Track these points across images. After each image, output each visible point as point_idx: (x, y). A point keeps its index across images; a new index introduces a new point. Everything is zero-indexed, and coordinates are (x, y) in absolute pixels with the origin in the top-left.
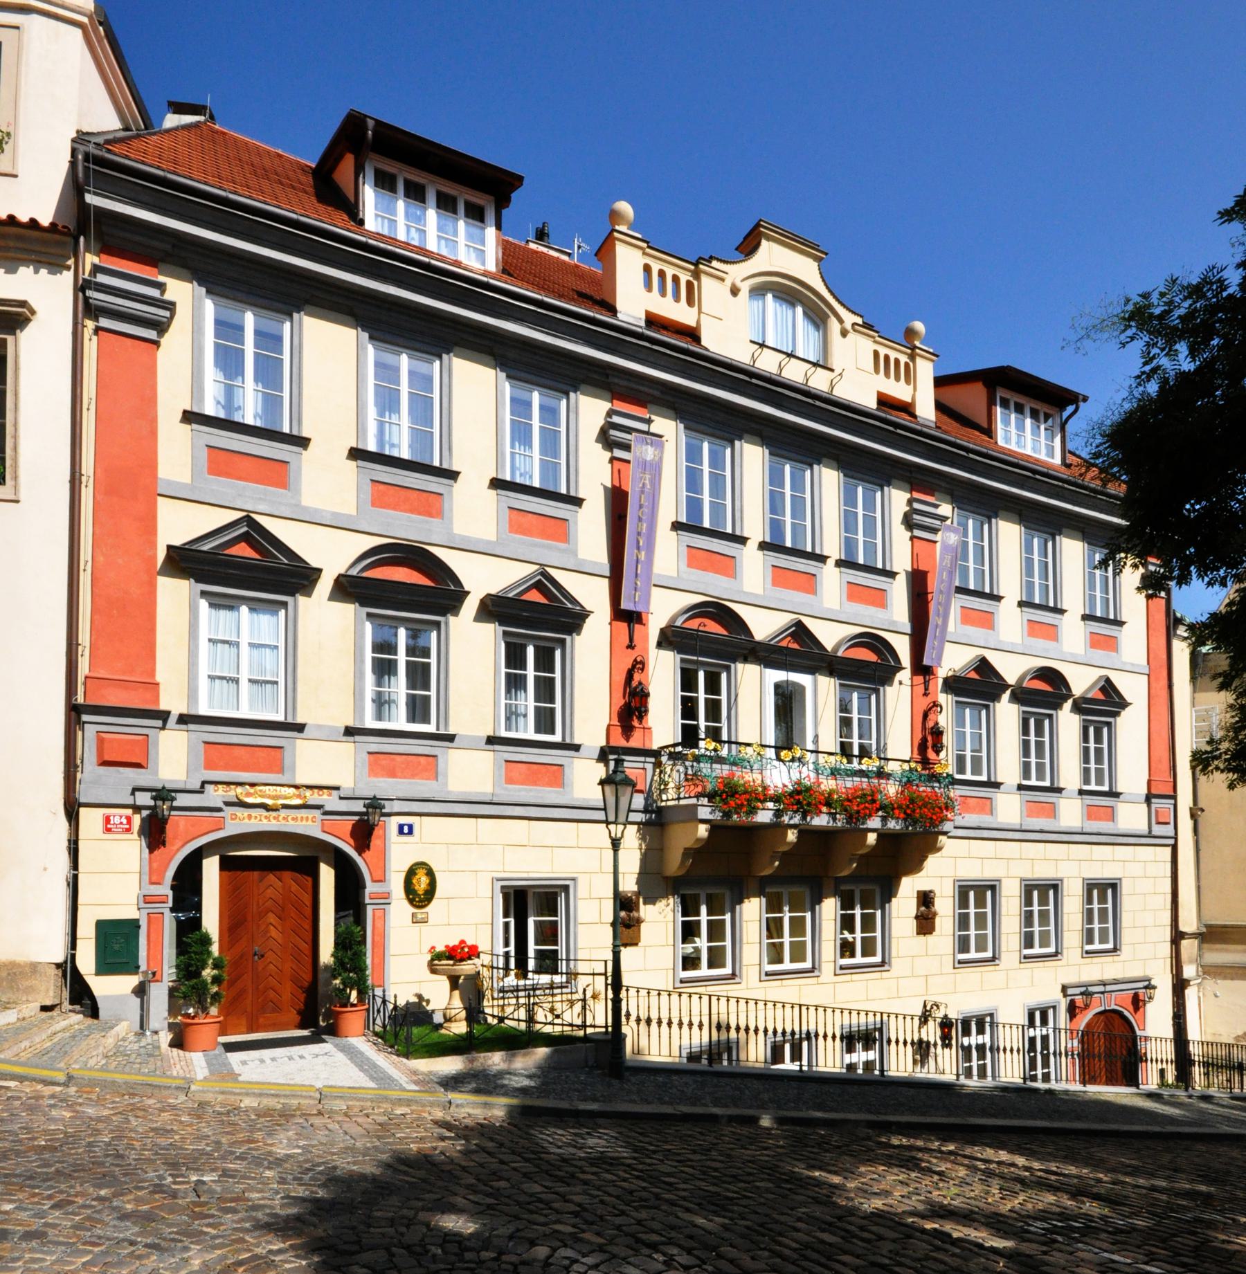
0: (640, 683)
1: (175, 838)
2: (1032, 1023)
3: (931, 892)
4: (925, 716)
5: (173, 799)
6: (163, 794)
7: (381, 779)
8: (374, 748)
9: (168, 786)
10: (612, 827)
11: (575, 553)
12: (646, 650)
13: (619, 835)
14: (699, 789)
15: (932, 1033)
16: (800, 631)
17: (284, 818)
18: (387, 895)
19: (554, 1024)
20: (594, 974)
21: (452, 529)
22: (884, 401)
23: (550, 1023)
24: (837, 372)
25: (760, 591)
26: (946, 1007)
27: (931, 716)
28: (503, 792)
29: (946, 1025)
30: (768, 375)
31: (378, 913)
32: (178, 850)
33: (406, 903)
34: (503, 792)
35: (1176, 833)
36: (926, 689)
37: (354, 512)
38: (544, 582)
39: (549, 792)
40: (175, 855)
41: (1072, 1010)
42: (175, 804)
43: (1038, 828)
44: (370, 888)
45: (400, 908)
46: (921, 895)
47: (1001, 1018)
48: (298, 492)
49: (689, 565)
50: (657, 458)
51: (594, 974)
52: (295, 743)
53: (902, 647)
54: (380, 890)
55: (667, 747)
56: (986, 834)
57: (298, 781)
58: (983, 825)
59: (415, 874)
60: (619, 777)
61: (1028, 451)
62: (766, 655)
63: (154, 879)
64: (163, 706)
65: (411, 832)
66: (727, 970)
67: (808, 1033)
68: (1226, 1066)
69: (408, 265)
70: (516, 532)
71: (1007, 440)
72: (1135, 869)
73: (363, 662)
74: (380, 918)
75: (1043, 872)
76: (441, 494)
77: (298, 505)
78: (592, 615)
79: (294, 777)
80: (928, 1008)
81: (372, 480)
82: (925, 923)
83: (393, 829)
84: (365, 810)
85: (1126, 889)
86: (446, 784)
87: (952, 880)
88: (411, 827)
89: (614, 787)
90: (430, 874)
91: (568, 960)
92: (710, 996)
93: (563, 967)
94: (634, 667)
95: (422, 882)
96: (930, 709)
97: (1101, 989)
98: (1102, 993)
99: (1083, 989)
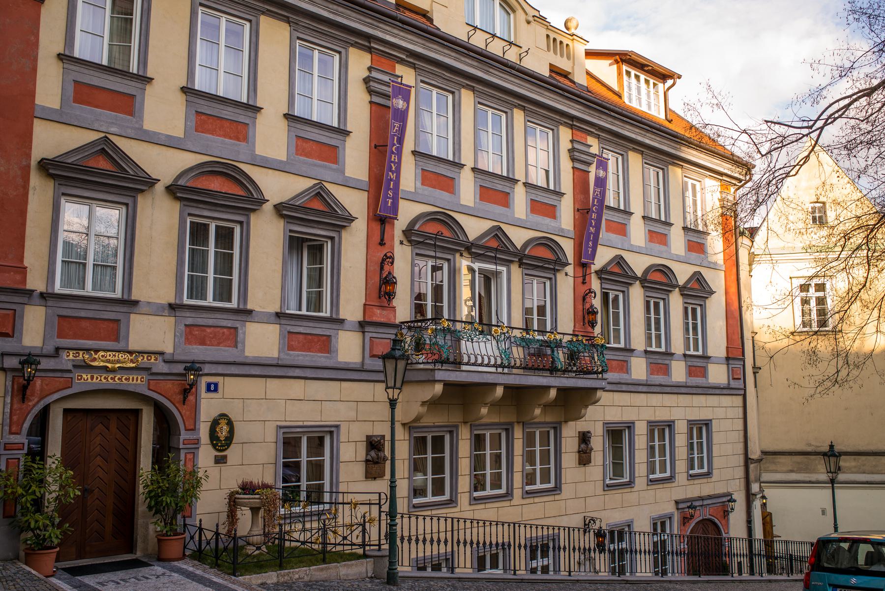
0: (390, 273)
1: (32, 395)
2: (655, 532)
3: (589, 432)
4: (584, 299)
5: (39, 363)
6: (30, 359)
7: (195, 347)
8: (189, 321)
9: (33, 352)
10: (390, 391)
11: (343, 172)
12: (392, 247)
13: (396, 397)
14: (436, 357)
15: (590, 541)
16: (497, 233)
17: (126, 379)
18: (197, 441)
19: (344, 545)
20: (370, 504)
21: (255, 152)
22: (553, 69)
23: (339, 544)
24: (525, 49)
25: (472, 204)
26: (601, 521)
27: (587, 300)
28: (286, 357)
29: (599, 534)
30: (481, 50)
31: (189, 456)
32: (34, 406)
33: (210, 447)
34: (286, 357)
35: (745, 386)
36: (584, 279)
37: (182, 136)
38: (320, 193)
39: (320, 357)
40: (32, 409)
41: (685, 520)
42: (39, 367)
43: (657, 383)
44: (184, 435)
45: (206, 455)
46: (581, 435)
47: (636, 528)
48: (141, 118)
49: (423, 184)
50: (405, 107)
51: (370, 504)
52: (129, 317)
53: (568, 247)
54: (191, 437)
55: (407, 322)
56: (624, 388)
57: (131, 347)
58: (623, 381)
59: (219, 424)
60: (398, 353)
61: (644, 108)
62: (473, 249)
63: (14, 429)
64: (29, 286)
65: (216, 390)
66: (447, 497)
67: (503, 544)
68: (780, 557)
69: (538, 107)
70: (301, 155)
71: (630, 100)
72: (720, 413)
73: (184, 252)
74: (190, 459)
75: (662, 415)
76: (248, 124)
77: (141, 129)
78: (356, 221)
79: (127, 344)
80: (587, 522)
81: (196, 111)
82: (584, 457)
83: (203, 387)
84: (184, 372)
85: (715, 426)
86: (243, 351)
87: (602, 422)
88: (216, 385)
89: (394, 361)
90: (230, 423)
91: (331, 492)
92: (452, 519)
93: (327, 497)
94: (383, 261)
95: (223, 431)
96: (587, 294)
97: (700, 503)
98: (702, 506)
99: (689, 504)
